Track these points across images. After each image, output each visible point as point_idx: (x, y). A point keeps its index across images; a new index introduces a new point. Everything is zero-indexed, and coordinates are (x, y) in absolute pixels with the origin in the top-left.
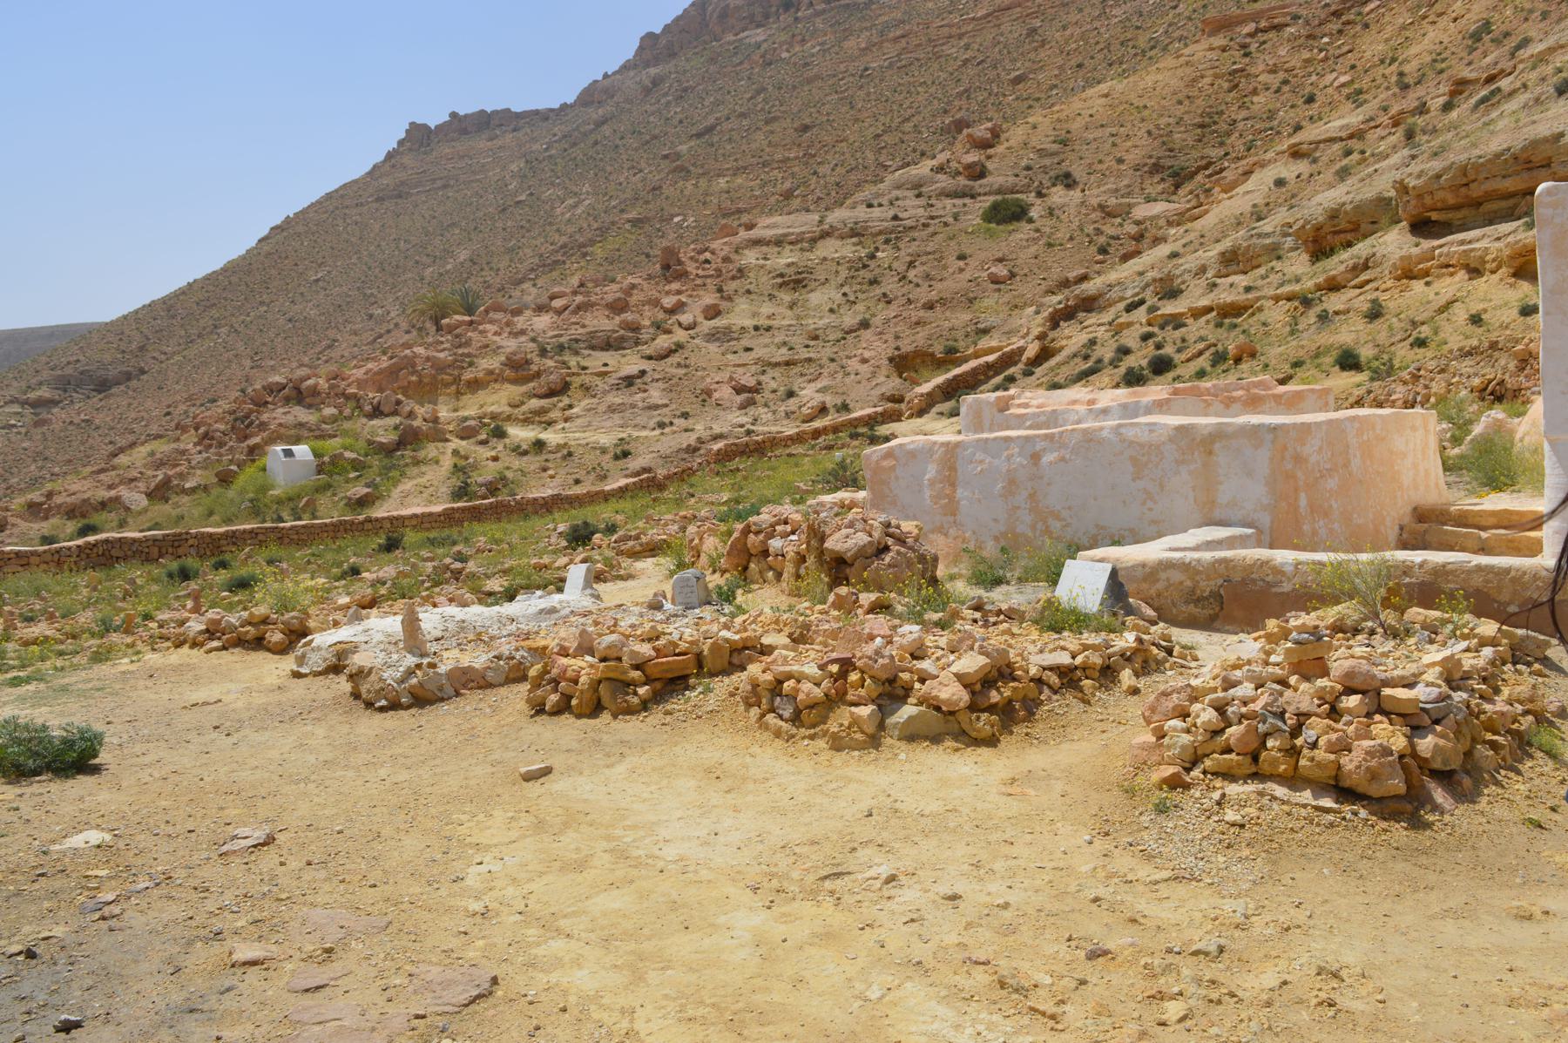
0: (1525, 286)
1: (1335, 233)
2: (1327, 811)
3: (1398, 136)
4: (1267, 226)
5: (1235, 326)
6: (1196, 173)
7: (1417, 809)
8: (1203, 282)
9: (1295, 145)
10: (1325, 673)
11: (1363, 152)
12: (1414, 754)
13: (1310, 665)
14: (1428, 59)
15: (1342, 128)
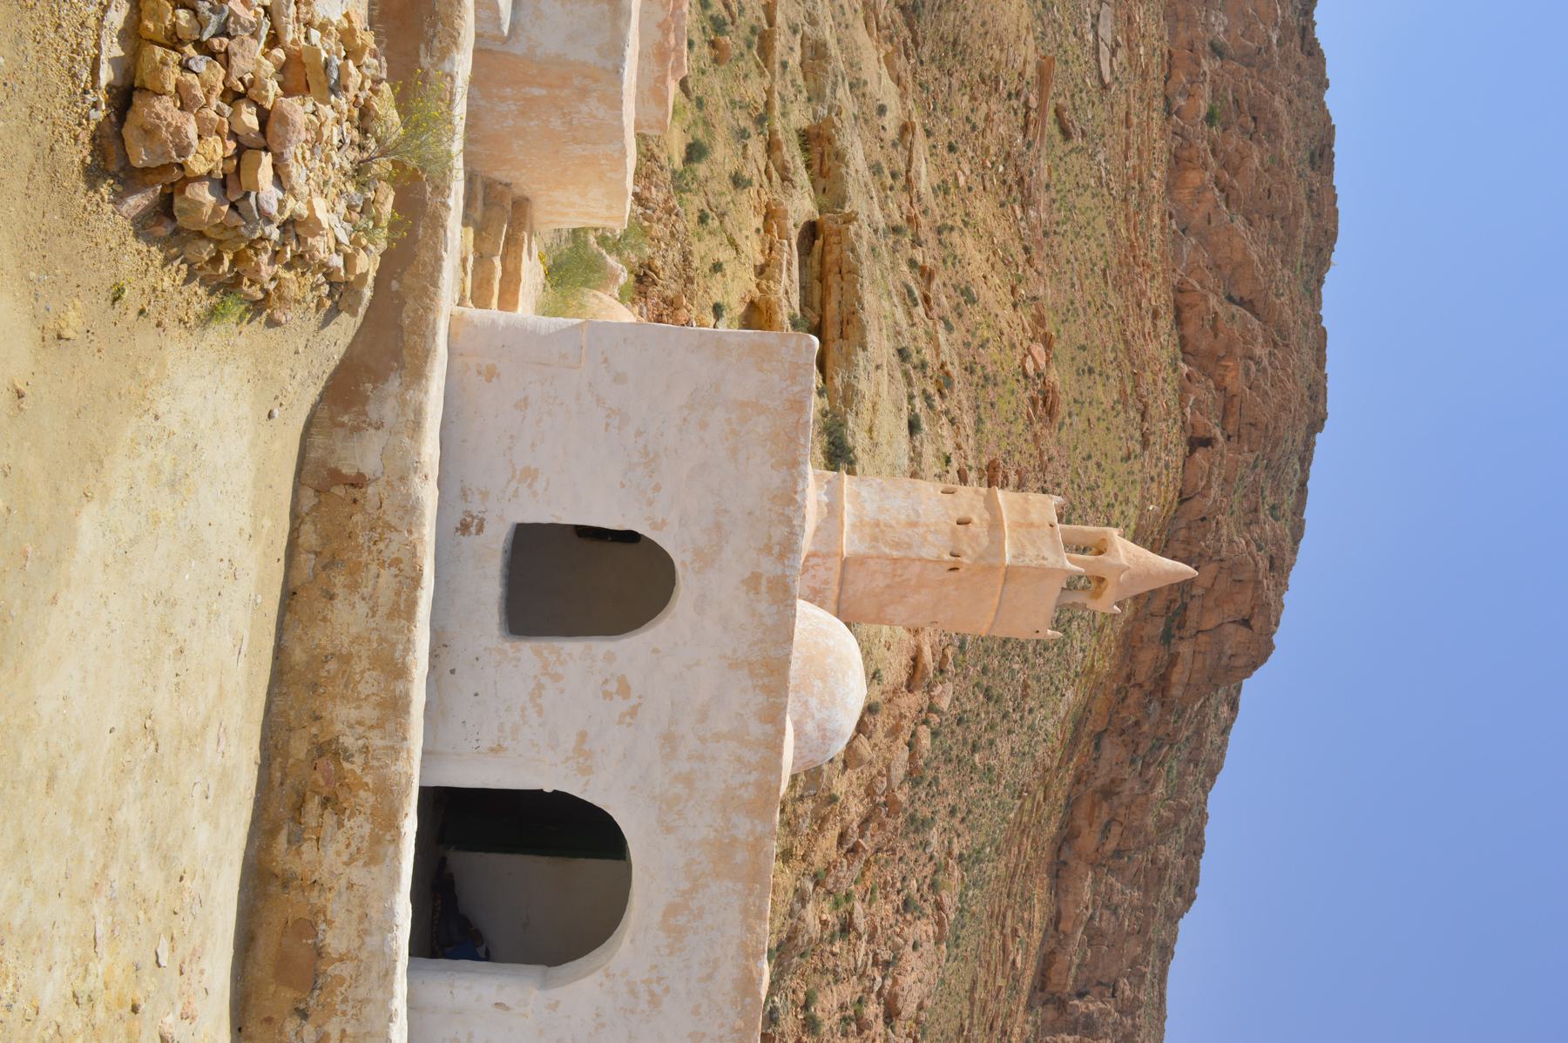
0: (740, 309)
1: (822, 155)
2: (95, 72)
3: (897, 219)
4: (843, 92)
5: (749, 47)
6: (911, 30)
7: (114, 176)
8: (800, 20)
9: (914, 129)
10: (288, 91)
11: (891, 188)
12: (188, 180)
13: (300, 75)
14: (958, 252)
15: (918, 173)
